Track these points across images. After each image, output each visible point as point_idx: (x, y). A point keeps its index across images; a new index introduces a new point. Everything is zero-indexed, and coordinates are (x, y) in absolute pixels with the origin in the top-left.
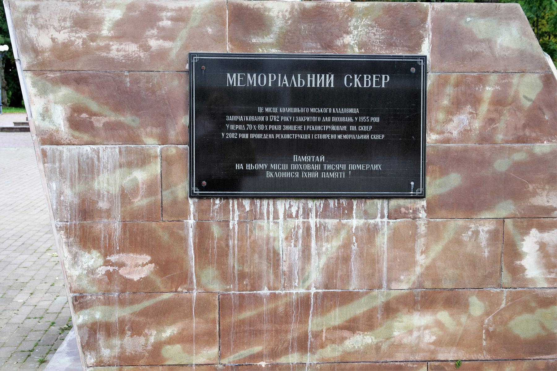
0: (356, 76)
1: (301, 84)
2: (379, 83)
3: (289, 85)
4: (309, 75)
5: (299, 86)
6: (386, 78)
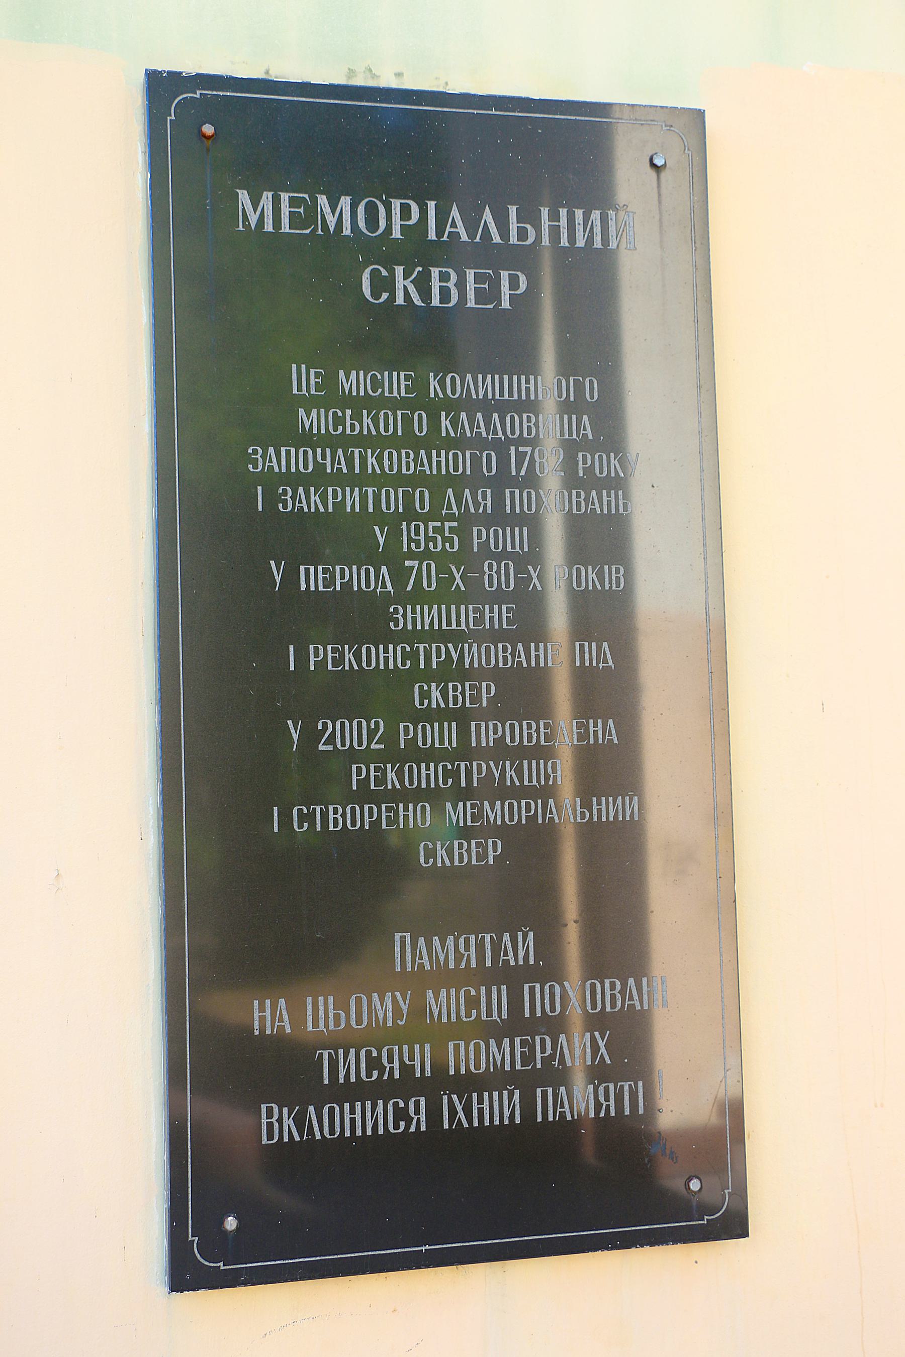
6: (495, 845)
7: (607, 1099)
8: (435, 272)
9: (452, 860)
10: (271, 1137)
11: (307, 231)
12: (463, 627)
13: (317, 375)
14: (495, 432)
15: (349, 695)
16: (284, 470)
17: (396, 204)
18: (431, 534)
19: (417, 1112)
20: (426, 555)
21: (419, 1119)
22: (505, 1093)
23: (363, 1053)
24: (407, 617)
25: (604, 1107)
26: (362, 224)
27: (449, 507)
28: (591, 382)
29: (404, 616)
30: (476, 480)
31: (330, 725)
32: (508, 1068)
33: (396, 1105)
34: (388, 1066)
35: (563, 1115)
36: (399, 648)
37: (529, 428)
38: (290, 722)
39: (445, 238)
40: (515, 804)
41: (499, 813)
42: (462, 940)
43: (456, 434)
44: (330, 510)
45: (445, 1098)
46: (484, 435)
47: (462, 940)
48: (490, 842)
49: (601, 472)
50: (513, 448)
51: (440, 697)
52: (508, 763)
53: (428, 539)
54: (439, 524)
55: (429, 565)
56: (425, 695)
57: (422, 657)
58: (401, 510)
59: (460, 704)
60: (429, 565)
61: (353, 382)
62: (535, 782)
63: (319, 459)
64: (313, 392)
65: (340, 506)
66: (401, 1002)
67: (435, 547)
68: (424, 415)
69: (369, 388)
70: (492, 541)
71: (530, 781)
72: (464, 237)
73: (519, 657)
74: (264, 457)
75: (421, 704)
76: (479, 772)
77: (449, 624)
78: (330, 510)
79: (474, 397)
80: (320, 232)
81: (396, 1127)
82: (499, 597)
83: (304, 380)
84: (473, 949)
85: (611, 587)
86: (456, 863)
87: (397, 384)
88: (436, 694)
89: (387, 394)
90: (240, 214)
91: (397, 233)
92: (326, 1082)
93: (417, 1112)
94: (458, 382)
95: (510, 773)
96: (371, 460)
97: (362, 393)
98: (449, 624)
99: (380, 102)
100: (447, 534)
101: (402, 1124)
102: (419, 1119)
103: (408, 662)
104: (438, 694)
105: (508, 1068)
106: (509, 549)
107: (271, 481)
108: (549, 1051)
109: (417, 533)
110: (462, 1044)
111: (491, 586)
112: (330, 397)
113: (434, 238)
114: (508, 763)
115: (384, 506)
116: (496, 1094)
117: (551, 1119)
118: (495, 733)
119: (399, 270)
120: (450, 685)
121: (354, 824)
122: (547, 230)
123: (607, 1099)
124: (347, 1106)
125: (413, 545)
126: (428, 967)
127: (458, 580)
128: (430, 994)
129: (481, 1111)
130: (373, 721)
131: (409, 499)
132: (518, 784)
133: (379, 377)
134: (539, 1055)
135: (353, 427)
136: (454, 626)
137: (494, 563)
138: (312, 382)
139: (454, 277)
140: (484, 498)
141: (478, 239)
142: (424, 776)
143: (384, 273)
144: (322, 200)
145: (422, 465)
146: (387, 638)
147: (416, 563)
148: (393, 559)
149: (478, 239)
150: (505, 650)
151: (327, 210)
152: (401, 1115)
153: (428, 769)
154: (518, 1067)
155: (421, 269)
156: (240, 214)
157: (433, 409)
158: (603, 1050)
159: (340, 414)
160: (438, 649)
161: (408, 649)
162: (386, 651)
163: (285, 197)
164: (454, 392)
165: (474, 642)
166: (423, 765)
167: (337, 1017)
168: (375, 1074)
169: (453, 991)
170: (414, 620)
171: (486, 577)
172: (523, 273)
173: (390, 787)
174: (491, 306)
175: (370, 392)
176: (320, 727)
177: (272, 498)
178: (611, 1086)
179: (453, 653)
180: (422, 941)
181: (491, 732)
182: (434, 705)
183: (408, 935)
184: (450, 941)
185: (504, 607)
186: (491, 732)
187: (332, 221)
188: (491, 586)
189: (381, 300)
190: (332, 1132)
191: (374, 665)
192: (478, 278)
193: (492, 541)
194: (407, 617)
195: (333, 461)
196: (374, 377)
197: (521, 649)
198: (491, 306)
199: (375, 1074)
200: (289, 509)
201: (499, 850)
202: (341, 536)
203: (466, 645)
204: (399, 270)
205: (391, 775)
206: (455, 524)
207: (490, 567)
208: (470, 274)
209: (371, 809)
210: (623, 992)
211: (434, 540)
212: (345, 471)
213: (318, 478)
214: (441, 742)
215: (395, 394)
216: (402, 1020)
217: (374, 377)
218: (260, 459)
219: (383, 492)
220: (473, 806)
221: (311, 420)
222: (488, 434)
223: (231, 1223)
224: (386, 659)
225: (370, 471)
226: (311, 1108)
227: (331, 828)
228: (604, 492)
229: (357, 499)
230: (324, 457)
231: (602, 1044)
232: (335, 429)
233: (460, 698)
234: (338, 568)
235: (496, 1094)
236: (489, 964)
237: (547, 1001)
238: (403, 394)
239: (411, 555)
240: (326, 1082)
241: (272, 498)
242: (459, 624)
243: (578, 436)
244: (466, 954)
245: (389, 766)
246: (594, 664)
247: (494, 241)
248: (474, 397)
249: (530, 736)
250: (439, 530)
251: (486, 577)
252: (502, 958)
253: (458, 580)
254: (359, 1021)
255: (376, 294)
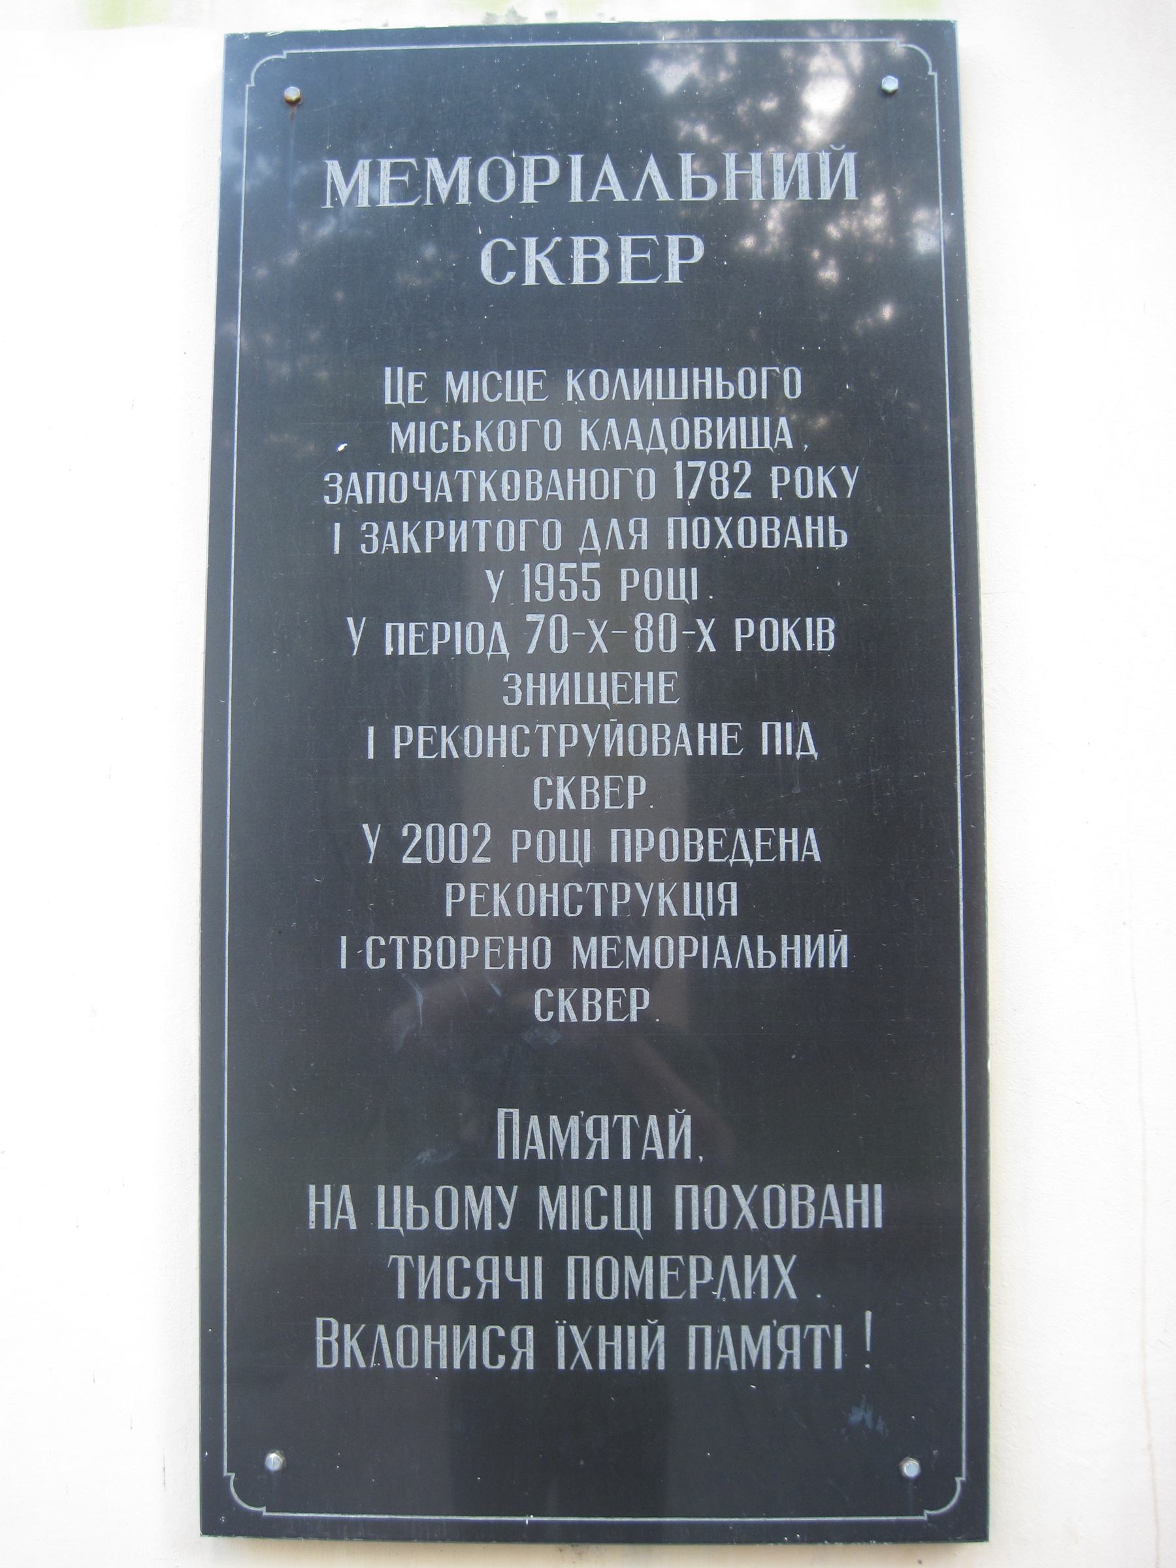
0: (562, 992)
1: (767, 959)
2: (622, 1010)
3: (733, 963)
4: (784, 938)
5: (761, 965)
6: (640, 996)
7: (789, 1345)
8: (579, 242)
9: (579, 1013)
10: (328, 1360)
11: (412, 203)
12: (604, 701)
13: (418, 380)
14: (655, 443)
15: (439, 791)
16: (369, 501)
17: (529, 162)
18: (563, 579)
19: (522, 1344)
20: (556, 606)
21: (524, 1355)
22: (645, 1329)
23: (451, 1262)
24: (525, 689)
25: (785, 1357)
26: (483, 189)
27: (589, 543)
28: (792, 374)
29: (523, 687)
30: (626, 507)
31: (418, 830)
32: (649, 1295)
33: (493, 1333)
34: (484, 1282)
35: (725, 1363)
36: (514, 730)
37: (703, 436)
38: (366, 827)
39: (594, 199)
40: (671, 941)
41: (647, 953)
42: (590, 1123)
43: (601, 446)
44: (429, 550)
45: (561, 1331)
46: (640, 447)
47: (590, 1123)
48: (634, 991)
49: (804, 492)
50: (679, 464)
51: (568, 796)
52: (661, 886)
53: (558, 585)
54: (574, 566)
55: (558, 621)
56: (549, 792)
57: (545, 742)
58: (522, 548)
59: (596, 806)
60: (558, 621)
61: (464, 386)
62: (699, 912)
63: (416, 486)
64: (411, 400)
65: (441, 545)
66: (642, 896)
67: (568, 596)
68: (558, 424)
69: (485, 392)
70: (647, 587)
71: (693, 909)
72: (619, 196)
73: (682, 742)
74: (344, 485)
75: (543, 804)
76: (621, 896)
77: (584, 697)
78: (429, 550)
79: (628, 398)
80: (428, 203)
81: (494, 1361)
82: (655, 661)
83: (399, 385)
84: (605, 1135)
85: (815, 647)
86: (586, 1018)
87: (523, 385)
88: (563, 791)
89: (508, 399)
90: (329, 188)
91: (529, 197)
92: (401, 1296)
93: (522, 1344)
94: (606, 379)
95: (664, 899)
96: (485, 485)
97: (476, 400)
98: (584, 697)
99: (513, 41)
100: (585, 579)
101: (502, 1359)
102: (524, 1355)
103: (527, 749)
104: (567, 791)
105: (649, 1295)
106: (671, 597)
107: (353, 515)
108: (708, 1277)
109: (544, 578)
110: (586, 1260)
111: (644, 646)
112: (434, 405)
113: (579, 199)
114: (661, 886)
115: (500, 543)
116: (631, 1330)
117: (708, 1367)
118: (645, 844)
119: (531, 243)
120: (584, 779)
121: (446, 961)
122: (733, 181)
123: (789, 1345)
124: (428, 1329)
125: (538, 594)
126: (541, 1155)
127: (598, 634)
128: (544, 1191)
129: (610, 1351)
130: (476, 826)
131: (534, 533)
132: (675, 914)
133: (499, 378)
134: (693, 1282)
135: (462, 443)
136: (591, 701)
137: (650, 616)
138: (411, 389)
139: (604, 247)
140: (638, 529)
141: (638, 198)
142: (543, 900)
143: (511, 247)
144: (434, 164)
145: (554, 489)
146: (502, 716)
147: (541, 618)
148: (512, 611)
149: (638, 198)
150: (661, 732)
151: (439, 174)
152: (500, 1346)
153: (549, 891)
154: (664, 1295)
155: (559, 239)
156: (329, 188)
157: (571, 415)
158: (786, 1280)
159: (445, 427)
160: (569, 732)
161: (527, 731)
162: (497, 734)
163: (386, 164)
164: (599, 392)
165: (618, 722)
166: (543, 887)
167: (417, 1214)
168: (467, 1292)
169: (576, 1190)
170: (536, 693)
171: (638, 635)
172: (698, 235)
173: (496, 914)
174: (653, 281)
175: (487, 398)
176: (405, 833)
177: (353, 538)
178: (796, 1329)
179: (589, 737)
180: (534, 1121)
181: (639, 843)
182: (560, 806)
183: (516, 1113)
184: (574, 1121)
185: (662, 675)
186: (639, 843)
187: (444, 189)
188: (644, 646)
189: (505, 281)
190: (408, 1360)
191: (479, 751)
192: (637, 247)
193: (647, 587)
194: (525, 689)
195: (433, 487)
196: (492, 378)
197: (685, 732)
198: (653, 281)
199: (467, 1292)
200: (375, 550)
201: (646, 1003)
202: (439, 585)
203: (607, 727)
204: (531, 243)
205: (499, 899)
206: (596, 565)
207: (644, 622)
208: (626, 243)
209: (470, 943)
210: (817, 1203)
211: (567, 587)
212: (449, 499)
213: (414, 510)
214: (569, 855)
215: (520, 398)
216: (504, 1223)
217: (492, 378)
218: (340, 489)
219: (500, 525)
220: (611, 943)
221: (406, 437)
222: (645, 446)
223: (274, 1460)
224: (497, 745)
225: (483, 499)
226: (381, 1329)
227: (416, 966)
228: (809, 519)
229: (464, 535)
230: (422, 483)
231: (784, 1272)
232: (438, 447)
233: (597, 797)
234: (435, 625)
235: (631, 1330)
236: (627, 1155)
237: (708, 1210)
238: (530, 398)
239: (535, 607)
240: (401, 1296)
241: (353, 538)
242: (597, 697)
243: (772, 444)
244: (596, 1141)
245: (497, 886)
246: (789, 752)
247: (661, 199)
248: (628, 398)
249: (694, 849)
250: (574, 574)
251: (638, 635)
252: (646, 1148)
253: (599, 639)
254: (447, 1221)
255: (498, 273)
